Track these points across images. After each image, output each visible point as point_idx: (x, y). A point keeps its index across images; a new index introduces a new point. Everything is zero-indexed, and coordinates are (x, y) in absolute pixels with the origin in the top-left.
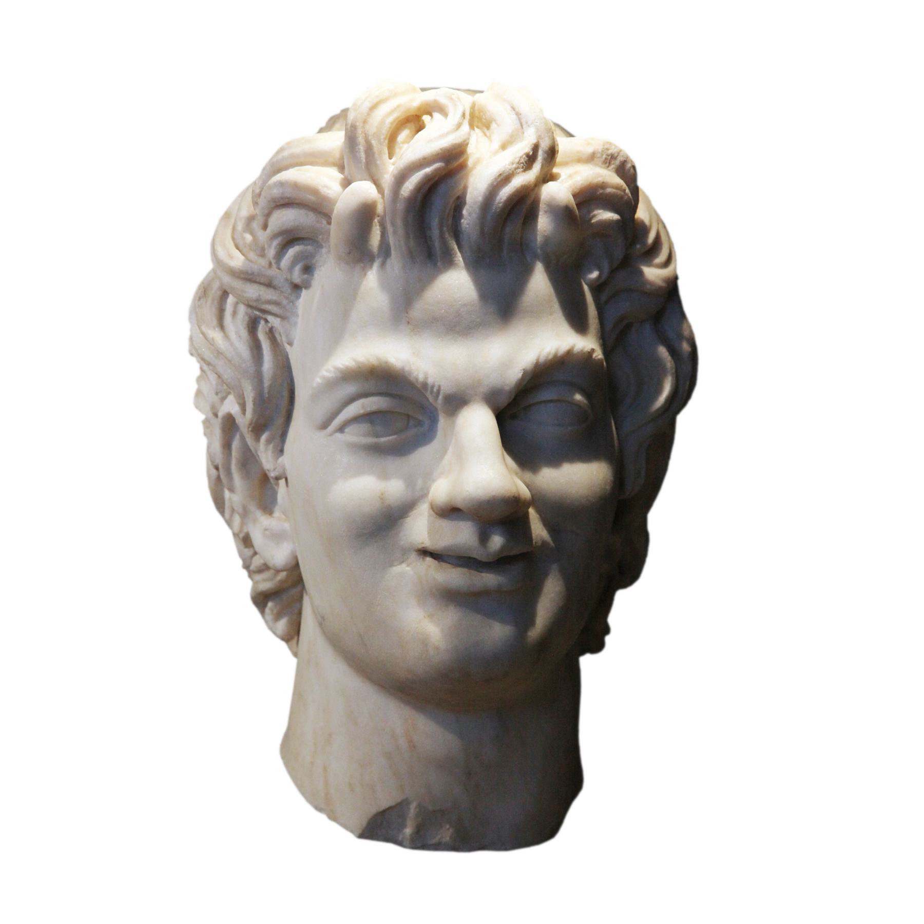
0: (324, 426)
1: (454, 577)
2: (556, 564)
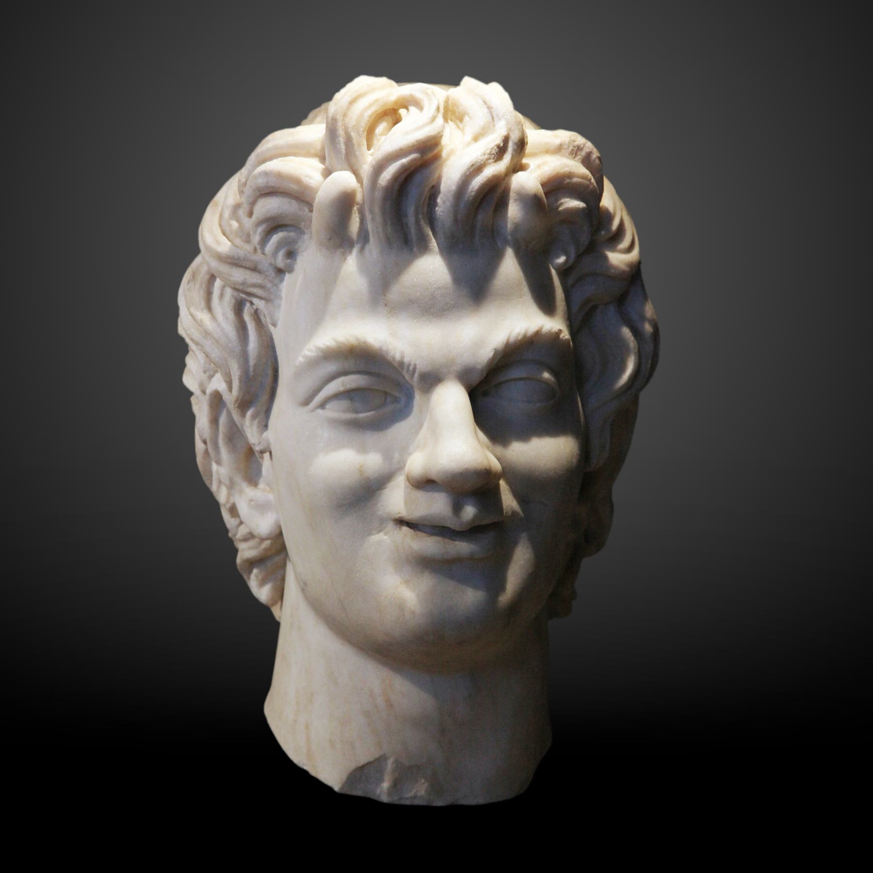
0: (306, 402)
1: (429, 545)
2: (525, 533)
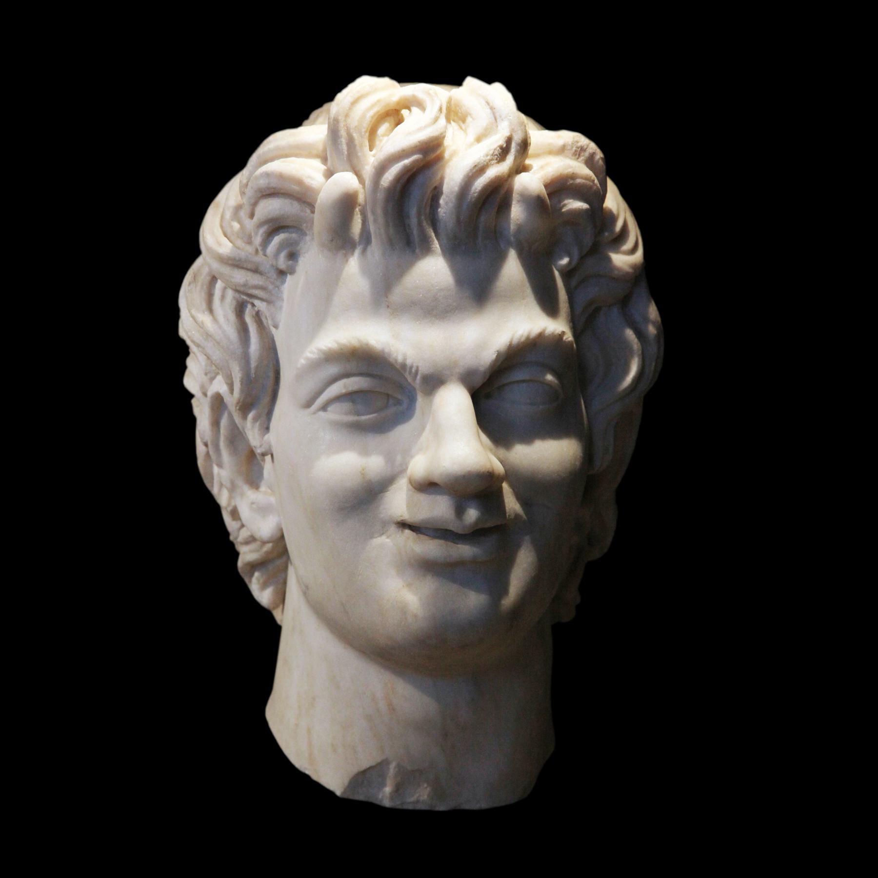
0: (308, 404)
1: (432, 548)
2: (528, 536)
